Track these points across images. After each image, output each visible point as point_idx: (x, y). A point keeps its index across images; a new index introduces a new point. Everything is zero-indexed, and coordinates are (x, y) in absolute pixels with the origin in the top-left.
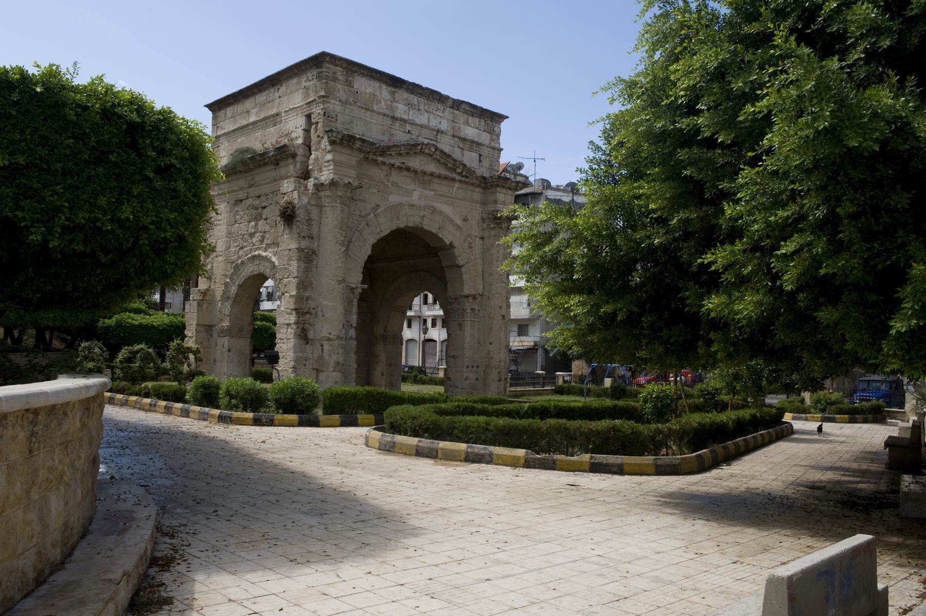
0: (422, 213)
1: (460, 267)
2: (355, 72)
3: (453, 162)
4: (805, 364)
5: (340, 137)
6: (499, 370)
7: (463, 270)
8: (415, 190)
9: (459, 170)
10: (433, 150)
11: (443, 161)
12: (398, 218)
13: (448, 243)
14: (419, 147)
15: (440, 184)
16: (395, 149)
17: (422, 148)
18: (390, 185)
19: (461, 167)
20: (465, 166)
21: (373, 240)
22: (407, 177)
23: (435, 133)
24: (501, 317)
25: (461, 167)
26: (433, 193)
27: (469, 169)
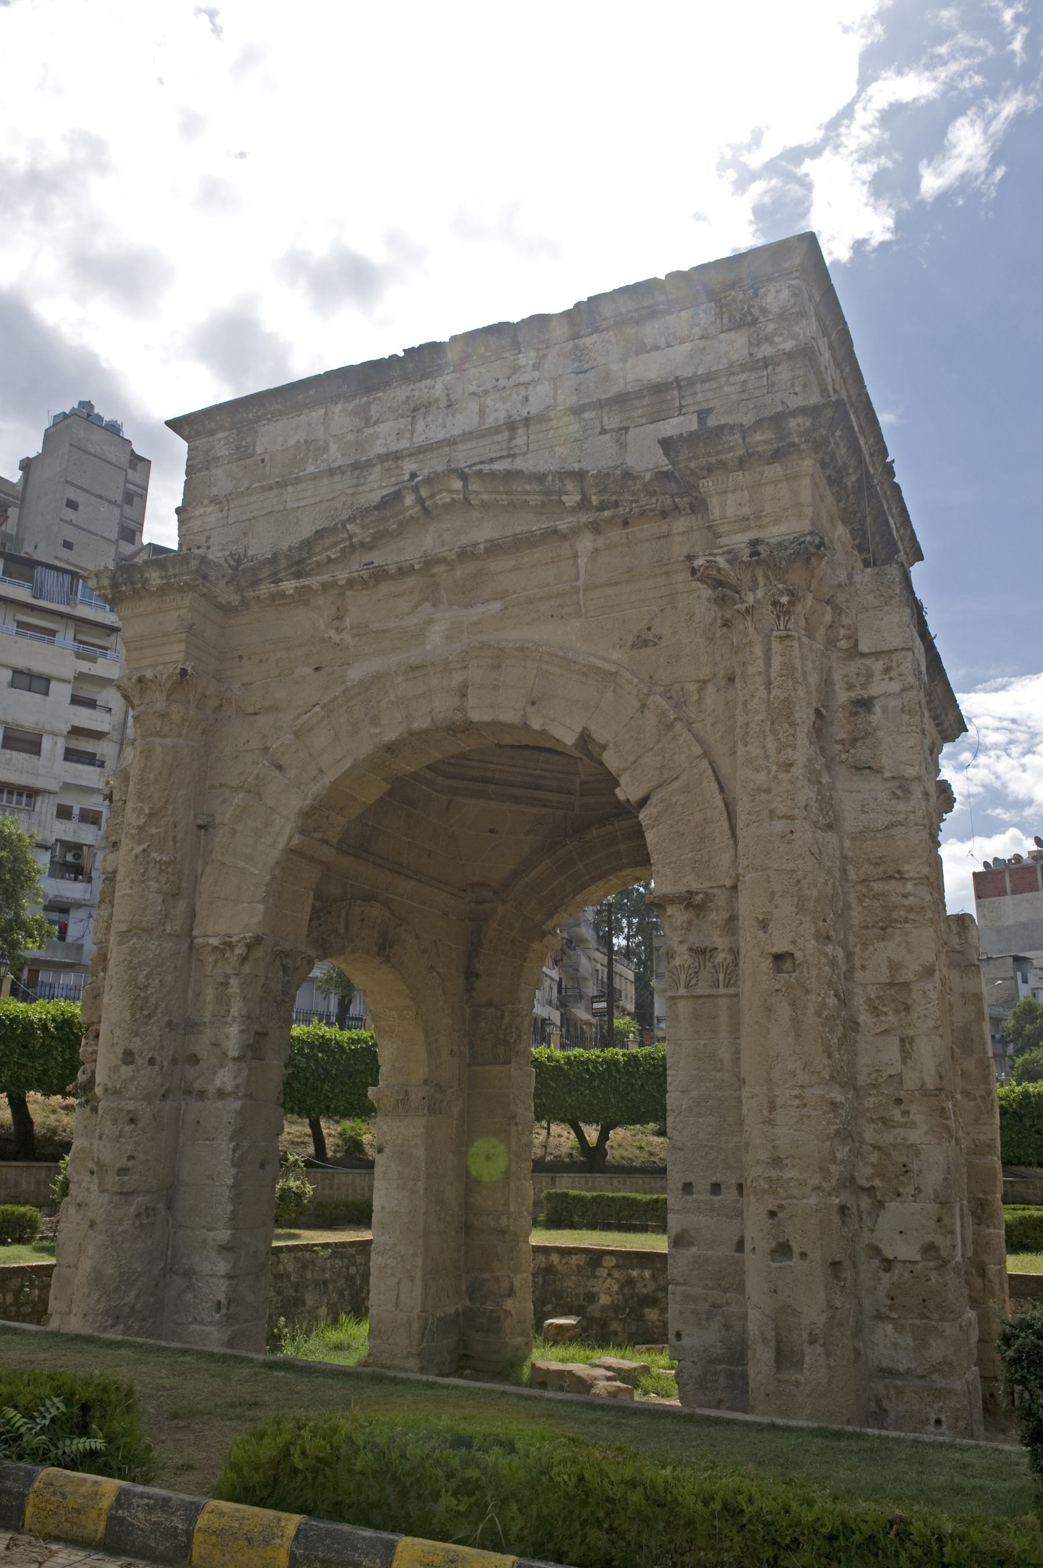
0: (457, 678)
1: (630, 810)
2: (258, 420)
3: (536, 487)
4: (801, 332)
5: (106, 582)
6: (771, 1203)
7: (644, 816)
8: (430, 622)
9: (572, 499)
10: (458, 484)
11: (505, 499)
12: (374, 721)
13: (569, 739)
14: (409, 500)
15: (517, 569)
16: (327, 542)
17: (421, 501)
18: (349, 640)
19: (570, 487)
20: (580, 476)
21: (296, 803)
22: (396, 596)
23: (506, 435)
24: (768, 963)
25: (570, 487)
26: (497, 606)
27: (603, 479)
